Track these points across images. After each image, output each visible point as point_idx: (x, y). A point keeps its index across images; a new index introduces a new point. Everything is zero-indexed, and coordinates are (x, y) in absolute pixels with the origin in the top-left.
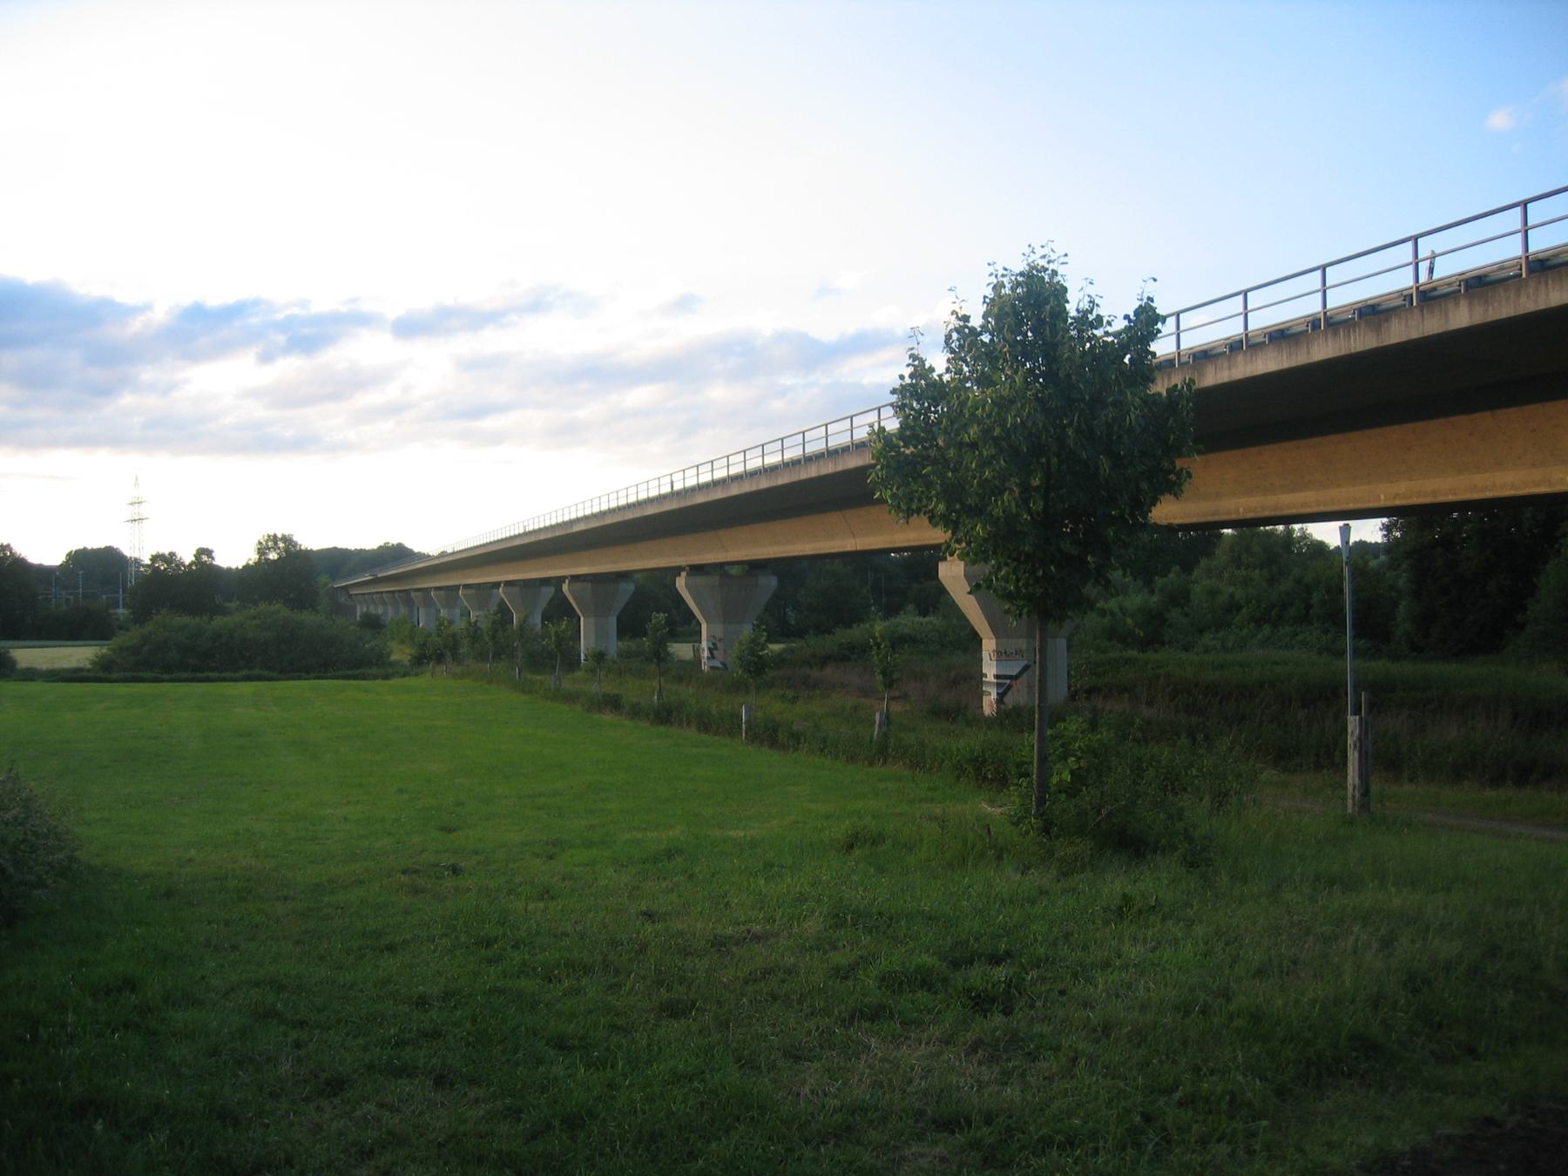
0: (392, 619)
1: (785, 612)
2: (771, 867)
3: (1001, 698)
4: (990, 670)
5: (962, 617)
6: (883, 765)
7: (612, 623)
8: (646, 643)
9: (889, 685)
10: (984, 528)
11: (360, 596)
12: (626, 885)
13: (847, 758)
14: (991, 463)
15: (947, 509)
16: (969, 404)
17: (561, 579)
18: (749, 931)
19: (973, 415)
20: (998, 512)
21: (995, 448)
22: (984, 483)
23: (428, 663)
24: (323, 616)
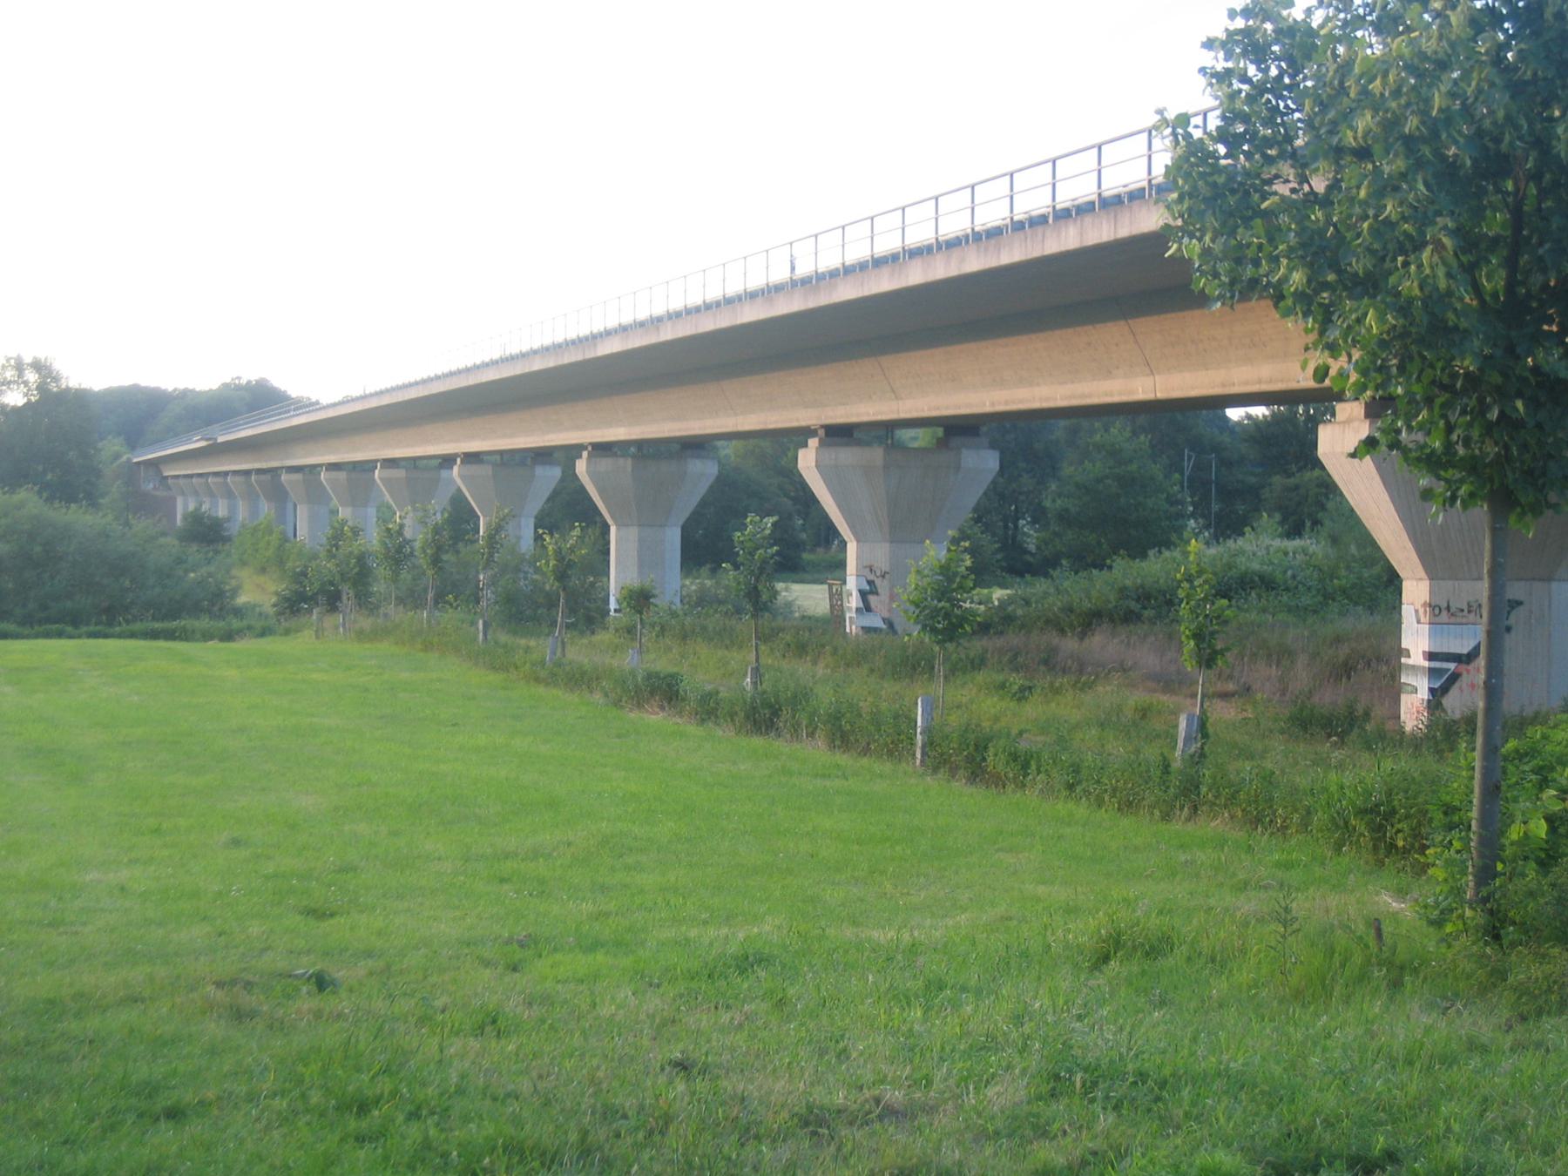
0: (243, 526)
1: (1016, 527)
2: (941, 989)
3: (1437, 694)
4: (1416, 640)
5: (1367, 541)
6: (1188, 820)
7: (673, 537)
8: (730, 576)
9: (1207, 659)
10: (1381, 319)
11: (181, 481)
12: (651, 1017)
13: (1119, 803)
14: (1396, 189)
15: (1309, 281)
16: (1357, 70)
17: (573, 451)
18: (877, 1101)
19: (1365, 92)
20: (1410, 287)
21: (1407, 157)
22: (1384, 227)
23: (310, 611)
24: (110, 517)
